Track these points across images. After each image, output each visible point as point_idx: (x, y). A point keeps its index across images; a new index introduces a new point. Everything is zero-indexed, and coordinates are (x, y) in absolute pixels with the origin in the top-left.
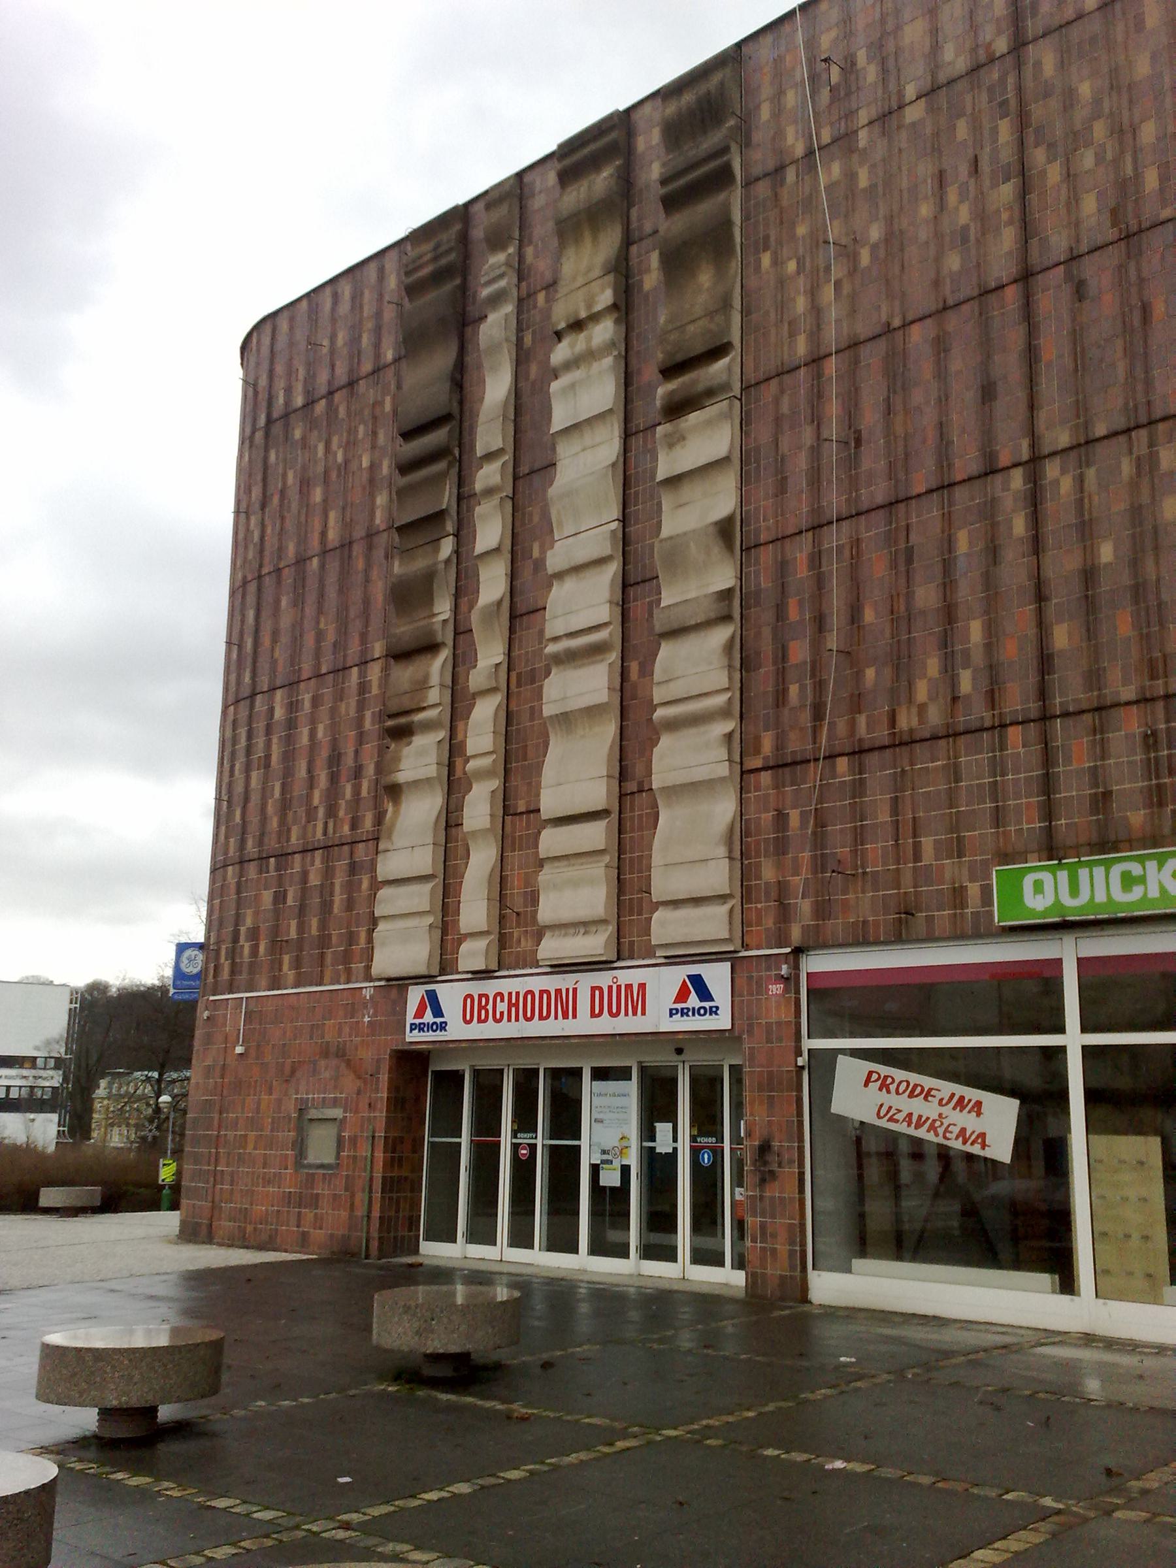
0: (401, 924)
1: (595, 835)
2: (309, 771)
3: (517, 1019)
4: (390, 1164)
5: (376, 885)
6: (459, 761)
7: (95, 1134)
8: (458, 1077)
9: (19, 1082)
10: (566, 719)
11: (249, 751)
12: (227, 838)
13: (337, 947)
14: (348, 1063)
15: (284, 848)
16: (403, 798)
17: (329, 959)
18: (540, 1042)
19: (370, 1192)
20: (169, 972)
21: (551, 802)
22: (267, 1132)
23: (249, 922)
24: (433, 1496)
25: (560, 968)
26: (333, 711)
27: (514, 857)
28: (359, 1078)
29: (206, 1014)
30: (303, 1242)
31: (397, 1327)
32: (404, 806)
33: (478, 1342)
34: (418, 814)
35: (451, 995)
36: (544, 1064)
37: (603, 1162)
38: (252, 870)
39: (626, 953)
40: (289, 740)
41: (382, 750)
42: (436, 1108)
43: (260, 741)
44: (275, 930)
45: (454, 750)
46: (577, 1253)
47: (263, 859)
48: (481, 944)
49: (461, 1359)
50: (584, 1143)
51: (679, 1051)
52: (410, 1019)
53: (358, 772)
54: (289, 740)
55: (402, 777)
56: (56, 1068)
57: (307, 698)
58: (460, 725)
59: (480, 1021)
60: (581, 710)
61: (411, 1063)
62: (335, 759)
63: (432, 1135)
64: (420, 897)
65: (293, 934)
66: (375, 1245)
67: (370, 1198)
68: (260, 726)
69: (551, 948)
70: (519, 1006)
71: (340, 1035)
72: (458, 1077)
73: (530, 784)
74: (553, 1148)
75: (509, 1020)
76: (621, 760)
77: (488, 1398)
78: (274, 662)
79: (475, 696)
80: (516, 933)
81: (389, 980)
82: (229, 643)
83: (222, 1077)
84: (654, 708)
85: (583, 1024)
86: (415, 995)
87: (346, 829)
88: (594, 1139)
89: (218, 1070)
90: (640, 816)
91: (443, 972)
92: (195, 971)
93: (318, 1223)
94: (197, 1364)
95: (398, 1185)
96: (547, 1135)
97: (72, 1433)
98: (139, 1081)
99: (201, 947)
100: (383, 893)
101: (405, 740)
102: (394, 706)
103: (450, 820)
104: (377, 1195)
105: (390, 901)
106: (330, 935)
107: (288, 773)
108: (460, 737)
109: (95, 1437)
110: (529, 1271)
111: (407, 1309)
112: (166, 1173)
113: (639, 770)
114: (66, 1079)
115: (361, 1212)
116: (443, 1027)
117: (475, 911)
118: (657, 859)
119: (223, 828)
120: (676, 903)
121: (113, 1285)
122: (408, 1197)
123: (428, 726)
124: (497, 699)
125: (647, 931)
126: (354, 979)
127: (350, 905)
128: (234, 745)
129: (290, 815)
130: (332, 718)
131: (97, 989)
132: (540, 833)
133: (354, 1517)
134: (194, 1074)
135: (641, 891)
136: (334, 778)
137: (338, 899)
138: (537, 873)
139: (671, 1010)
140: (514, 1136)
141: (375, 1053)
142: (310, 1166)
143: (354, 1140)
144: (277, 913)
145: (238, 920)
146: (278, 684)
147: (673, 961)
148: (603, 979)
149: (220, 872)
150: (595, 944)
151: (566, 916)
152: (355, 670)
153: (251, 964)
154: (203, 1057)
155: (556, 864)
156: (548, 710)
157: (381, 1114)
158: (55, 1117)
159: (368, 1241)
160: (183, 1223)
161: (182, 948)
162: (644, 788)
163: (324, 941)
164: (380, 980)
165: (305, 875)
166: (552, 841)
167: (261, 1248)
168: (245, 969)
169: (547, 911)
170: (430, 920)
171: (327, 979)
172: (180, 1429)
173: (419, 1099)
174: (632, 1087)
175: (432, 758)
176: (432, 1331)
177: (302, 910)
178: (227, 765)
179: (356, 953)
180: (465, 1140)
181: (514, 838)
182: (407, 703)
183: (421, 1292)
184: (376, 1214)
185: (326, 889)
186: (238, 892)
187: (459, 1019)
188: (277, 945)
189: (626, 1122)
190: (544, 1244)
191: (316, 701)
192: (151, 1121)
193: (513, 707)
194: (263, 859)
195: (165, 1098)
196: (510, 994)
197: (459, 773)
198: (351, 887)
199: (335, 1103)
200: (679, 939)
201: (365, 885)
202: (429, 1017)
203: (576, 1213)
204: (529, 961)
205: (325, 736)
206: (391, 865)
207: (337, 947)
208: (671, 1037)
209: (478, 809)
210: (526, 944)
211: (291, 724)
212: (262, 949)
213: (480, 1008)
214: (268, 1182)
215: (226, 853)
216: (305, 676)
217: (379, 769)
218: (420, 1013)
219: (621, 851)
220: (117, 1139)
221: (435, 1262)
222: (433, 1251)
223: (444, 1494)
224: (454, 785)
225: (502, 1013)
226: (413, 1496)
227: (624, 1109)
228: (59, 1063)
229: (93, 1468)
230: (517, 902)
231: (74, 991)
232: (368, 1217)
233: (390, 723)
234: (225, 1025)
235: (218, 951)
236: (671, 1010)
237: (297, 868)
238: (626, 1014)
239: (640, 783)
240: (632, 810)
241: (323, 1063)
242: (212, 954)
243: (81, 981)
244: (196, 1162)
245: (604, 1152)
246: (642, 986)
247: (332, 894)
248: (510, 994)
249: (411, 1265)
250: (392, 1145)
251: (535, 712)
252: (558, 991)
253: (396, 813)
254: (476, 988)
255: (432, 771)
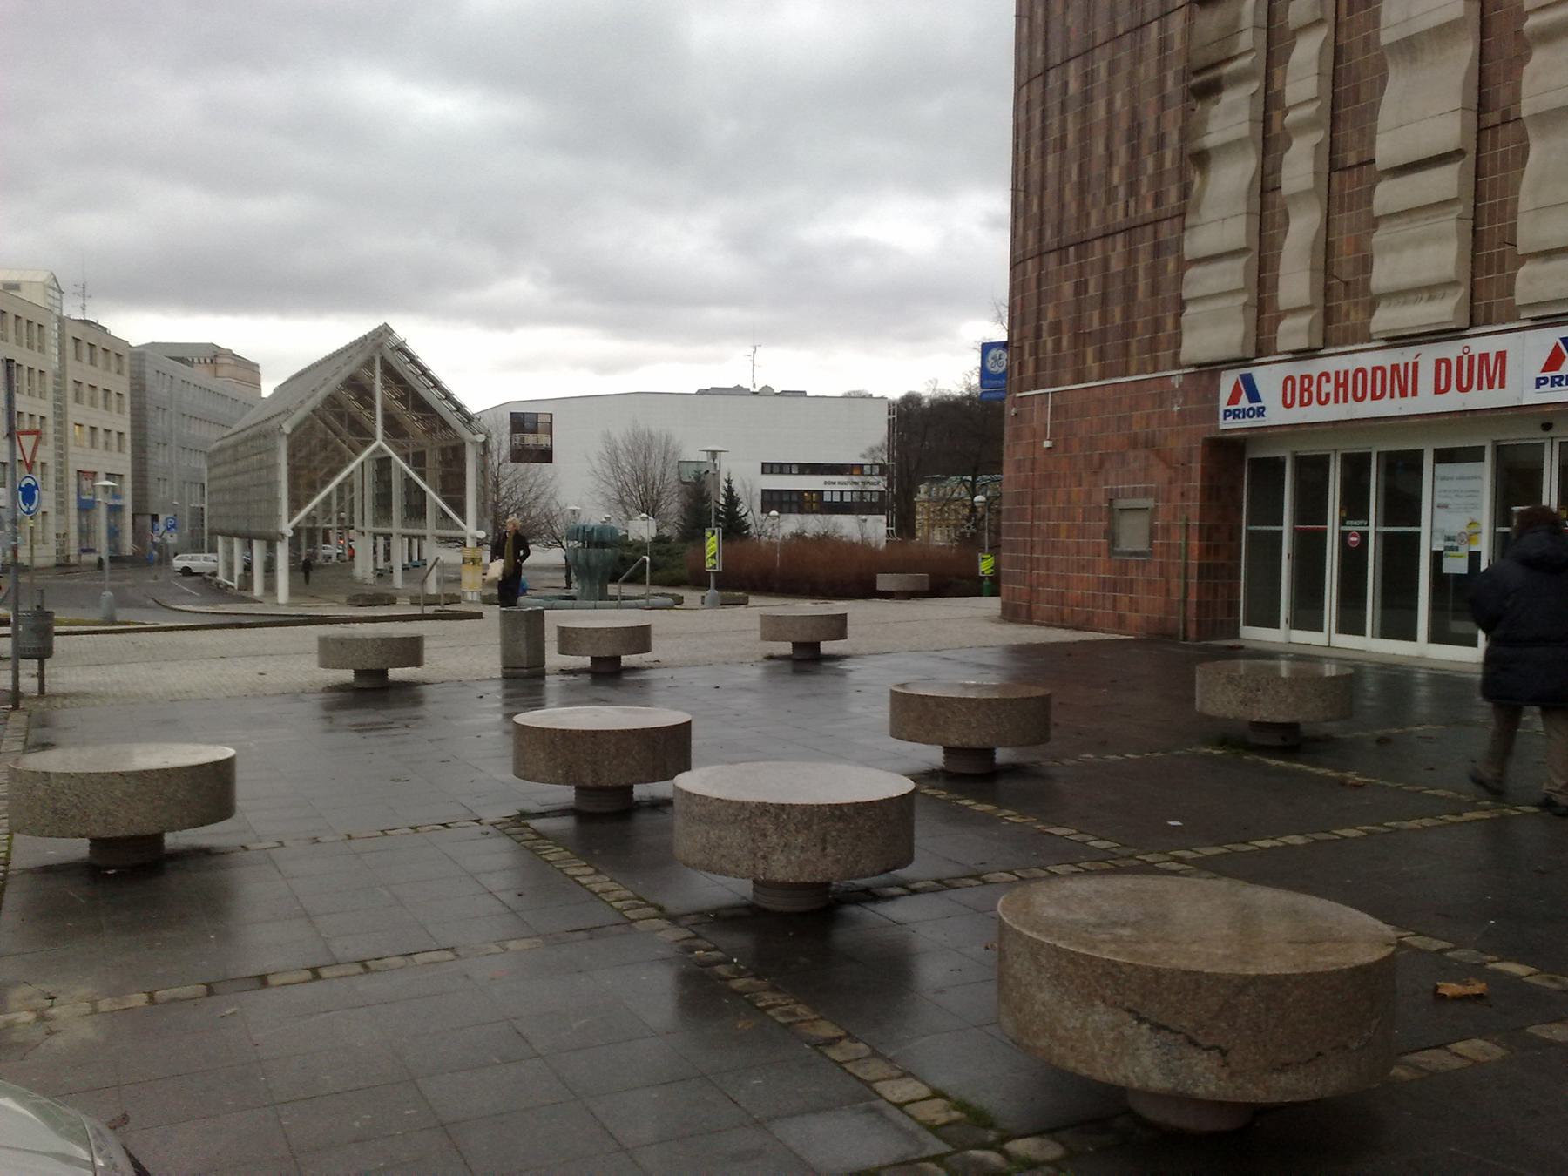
0: (1211, 306)
1: (1445, 182)
2: (1108, 147)
3: (1345, 401)
4: (1206, 551)
5: (1183, 265)
6: (1276, 114)
7: (919, 534)
8: (1278, 464)
9: (850, 488)
10: (1409, 46)
11: (1043, 136)
12: (1025, 230)
13: (1142, 334)
14: (1158, 453)
15: (1087, 235)
16: (1212, 164)
17: (1134, 348)
18: (1372, 423)
19: (1186, 577)
20: (975, 381)
21: (1388, 150)
22: (1079, 522)
23: (1050, 316)
24: (1266, 844)
25: (1396, 341)
26: (1132, 75)
27: (1343, 220)
28: (1170, 467)
29: (1014, 411)
30: (1120, 623)
31: (1219, 696)
32: (1212, 175)
33: (1308, 713)
34: (1230, 181)
35: (1268, 378)
36: (1377, 447)
37: (1447, 548)
38: (1051, 261)
39: (1481, 314)
40: (1085, 114)
41: (1187, 113)
42: (1254, 500)
43: (1055, 121)
44: (1077, 323)
45: (1271, 101)
46: (1415, 640)
47: (1062, 249)
48: (1303, 321)
49: (1292, 727)
50: (1425, 530)
51: (1547, 427)
52: (1223, 405)
53: (1160, 142)
54: (1085, 114)
55: (1211, 140)
56: (881, 474)
57: (1102, 66)
58: (1278, 71)
59: (1302, 404)
60: (1428, 31)
61: (1226, 454)
62: (1135, 129)
63: (1250, 523)
64: (1233, 274)
65: (1096, 325)
66: (1192, 628)
67: (1186, 585)
68: (1054, 104)
69: (1387, 319)
70: (1347, 386)
71: (1148, 425)
72: (1278, 464)
73: (1363, 129)
74: (1386, 534)
75: (1336, 401)
76: (1480, 87)
77: (1318, 765)
78: (1067, 30)
79: (1295, 33)
80: (1344, 304)
81: (1199, 366)
82: (1018, 16)
83: (1032, 470)
84: (1524, 16)
85: (1426, 401)
86: (1228, 381)
87: (1149, 207)
88: (1437, 525)
89: (1028, 464)
90: (1504, 154)
91: (1259, 353)
92: (1001, 370)
93: (1134, 606)
94: (1029, 715)
95: (1215, 571)
96: (1381, 519)
97: (925, 767)
98: (954, 487)
99: (1004, 345)
100: (1191, 273)
101: (1213, 99)
102: (1199, 60)
103: (1266, 186)
104: (1193, 581)
105: (1200, 281)
106: (1134, 324)
107: (1085, 152)
108: (1277, 86)
109: (942, 770)
110: (1361, 656)
111: (1231, 680)
112: (985, 566)
113: (1504, 95)
114: (890, 484)
115: (1177, 596)
116: (1260, 412)
117: (1295, 284)
118: (1525, 201)
119: (1021, 221)
120: (1548, 254)
121: (946, 654)
122: (1225, 584)
123: (1239, 78)
124: (1324, 32)
125: (1510, 291)
126: (1160, 367)
127: (1155, 290)
128: (1028, 128)
129: (1089, 199)
130: (1130, 84)
131: (911, 400)
132: (1373, 188)
133: (1188, 854)
134: (1008, 470)
135: (1503, 243)
136: (1134, 153)
137: (1142, 285)
138: (1370, 235)
139: (1538, 379)
140: (1342, 523)
141: (1185, 443)
142: (1122, 553)
143: (1167, 530)
144: (1079, 307)
145: (1040, 315)
146: (1072, 54)
147: (1541, 323)
148: (1452, 350)
149: (1019, 269)
150: (1443, 311)
151: (1406, 279)
152: (1155, 25)
153: (1055, 359)
154: (1012, 454)
155: (1396, 222)
156: (1386, 37)
157: (1194, 505)
158: (884, 518)
159: (1185, 625)
160: (1005, 607)
161: (986, 348)
162: (1510, 118)
163: (1128, 330)
164: (1190, 366)
165: (1106, 262)
166: (1388, 195)
167: (1077, 628)
168: (1049, 365)
169: (1381, 278)
170: (1244, 298)
171: (1133, 369)
172: (1014, 770)
173: (1235, 490)
174: (1484, 472)
175: (1244, 114)
176: (1258, 701)
177: (1104, 299)
178: (1022, 153)
179: (1162, 338)
180: (1287, 528)
181: (1342, 197)
182: (1215, 56)
183: (1243, 666)
184: (1193, 598)
185: (1129, 275)
186: (1039, 285)
187: (1276, 402)
188: (1079, 338)
189: (1476, 506)
190: (1377, 630)
191: (1112, 69)
192: (968, 520)
193: (1343, 41)
194: (1062, 249)
195: (979, 498)
196: (1337, 373)
197: (1276, 128)
198: (1155, 271)
199: (1146, 493)
200: (1551, 296)
201: (1171, 266)
202: (1244, 402)
203: (1415, 608)
204: (1360, 335)
205: (1123, 105)
206: (1200, 241)
207: (1142, 334)
208: (1536, 410)
209: (1300, 168)
210: (1356, 317)
211: (1087, 97)
212: (1065, 343)
213: (1303, 390)
214: (1082, 567)
215: (1024, 246)
216: (1099, 41)
217: (1185, 136)
218: (1234, 399)
219: (1478, 196)
220: (939, 538)
221: (1255, 645)
222: (1254, 635)
223: (1275, 843)
224: (1270, 141)
225: (1328, 395)
226: (1245, 843)
227: (1474, 493)
228: (883, 470)
229: (943, 795)
230: (1346, 271)
231: (891, 404)
232: (1185, 602)
233: (1195, 81)
234: (1032, 420)
235: (1021, 348)
236: (1538, 379)
237: (1098, 255)
238: (1480, 388)
239: (1506, 113)
240: (1494, 146)
241: (1131, 454)
242: (1016, 351)
243: (896, 394)
244: (1013, 551)
245: (1449, 539)
246: (1501, 356)
247: (1135, 280)
248: (1337, 373)
249: (1232, 648)
250: (1207, 533)
251: (1370, 43)
252: (1395, 368)
253: (1204, 183)
254: (1297, 369)
255: (1244, 130)
